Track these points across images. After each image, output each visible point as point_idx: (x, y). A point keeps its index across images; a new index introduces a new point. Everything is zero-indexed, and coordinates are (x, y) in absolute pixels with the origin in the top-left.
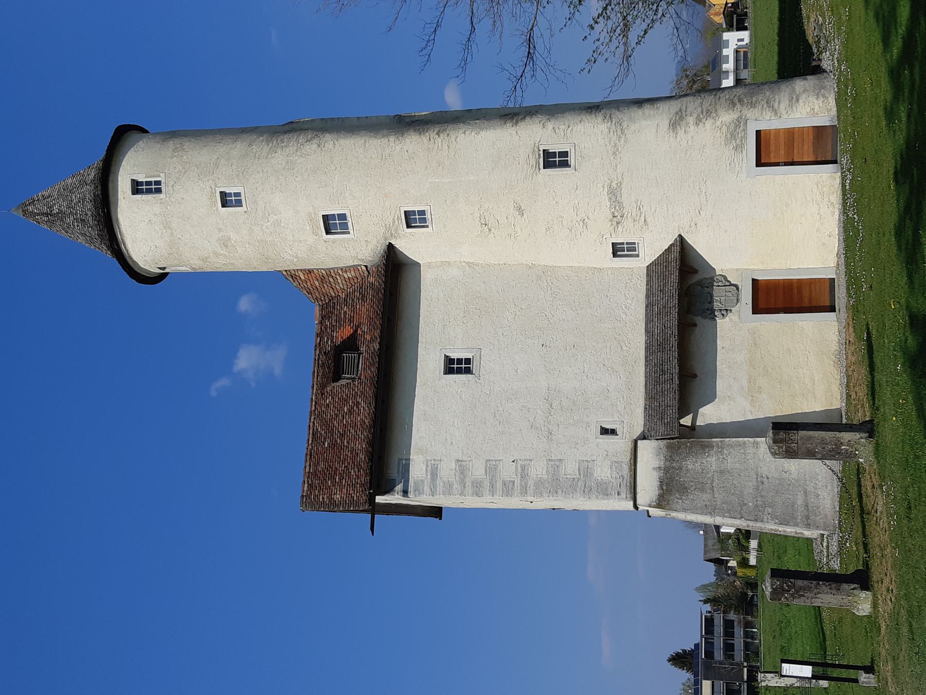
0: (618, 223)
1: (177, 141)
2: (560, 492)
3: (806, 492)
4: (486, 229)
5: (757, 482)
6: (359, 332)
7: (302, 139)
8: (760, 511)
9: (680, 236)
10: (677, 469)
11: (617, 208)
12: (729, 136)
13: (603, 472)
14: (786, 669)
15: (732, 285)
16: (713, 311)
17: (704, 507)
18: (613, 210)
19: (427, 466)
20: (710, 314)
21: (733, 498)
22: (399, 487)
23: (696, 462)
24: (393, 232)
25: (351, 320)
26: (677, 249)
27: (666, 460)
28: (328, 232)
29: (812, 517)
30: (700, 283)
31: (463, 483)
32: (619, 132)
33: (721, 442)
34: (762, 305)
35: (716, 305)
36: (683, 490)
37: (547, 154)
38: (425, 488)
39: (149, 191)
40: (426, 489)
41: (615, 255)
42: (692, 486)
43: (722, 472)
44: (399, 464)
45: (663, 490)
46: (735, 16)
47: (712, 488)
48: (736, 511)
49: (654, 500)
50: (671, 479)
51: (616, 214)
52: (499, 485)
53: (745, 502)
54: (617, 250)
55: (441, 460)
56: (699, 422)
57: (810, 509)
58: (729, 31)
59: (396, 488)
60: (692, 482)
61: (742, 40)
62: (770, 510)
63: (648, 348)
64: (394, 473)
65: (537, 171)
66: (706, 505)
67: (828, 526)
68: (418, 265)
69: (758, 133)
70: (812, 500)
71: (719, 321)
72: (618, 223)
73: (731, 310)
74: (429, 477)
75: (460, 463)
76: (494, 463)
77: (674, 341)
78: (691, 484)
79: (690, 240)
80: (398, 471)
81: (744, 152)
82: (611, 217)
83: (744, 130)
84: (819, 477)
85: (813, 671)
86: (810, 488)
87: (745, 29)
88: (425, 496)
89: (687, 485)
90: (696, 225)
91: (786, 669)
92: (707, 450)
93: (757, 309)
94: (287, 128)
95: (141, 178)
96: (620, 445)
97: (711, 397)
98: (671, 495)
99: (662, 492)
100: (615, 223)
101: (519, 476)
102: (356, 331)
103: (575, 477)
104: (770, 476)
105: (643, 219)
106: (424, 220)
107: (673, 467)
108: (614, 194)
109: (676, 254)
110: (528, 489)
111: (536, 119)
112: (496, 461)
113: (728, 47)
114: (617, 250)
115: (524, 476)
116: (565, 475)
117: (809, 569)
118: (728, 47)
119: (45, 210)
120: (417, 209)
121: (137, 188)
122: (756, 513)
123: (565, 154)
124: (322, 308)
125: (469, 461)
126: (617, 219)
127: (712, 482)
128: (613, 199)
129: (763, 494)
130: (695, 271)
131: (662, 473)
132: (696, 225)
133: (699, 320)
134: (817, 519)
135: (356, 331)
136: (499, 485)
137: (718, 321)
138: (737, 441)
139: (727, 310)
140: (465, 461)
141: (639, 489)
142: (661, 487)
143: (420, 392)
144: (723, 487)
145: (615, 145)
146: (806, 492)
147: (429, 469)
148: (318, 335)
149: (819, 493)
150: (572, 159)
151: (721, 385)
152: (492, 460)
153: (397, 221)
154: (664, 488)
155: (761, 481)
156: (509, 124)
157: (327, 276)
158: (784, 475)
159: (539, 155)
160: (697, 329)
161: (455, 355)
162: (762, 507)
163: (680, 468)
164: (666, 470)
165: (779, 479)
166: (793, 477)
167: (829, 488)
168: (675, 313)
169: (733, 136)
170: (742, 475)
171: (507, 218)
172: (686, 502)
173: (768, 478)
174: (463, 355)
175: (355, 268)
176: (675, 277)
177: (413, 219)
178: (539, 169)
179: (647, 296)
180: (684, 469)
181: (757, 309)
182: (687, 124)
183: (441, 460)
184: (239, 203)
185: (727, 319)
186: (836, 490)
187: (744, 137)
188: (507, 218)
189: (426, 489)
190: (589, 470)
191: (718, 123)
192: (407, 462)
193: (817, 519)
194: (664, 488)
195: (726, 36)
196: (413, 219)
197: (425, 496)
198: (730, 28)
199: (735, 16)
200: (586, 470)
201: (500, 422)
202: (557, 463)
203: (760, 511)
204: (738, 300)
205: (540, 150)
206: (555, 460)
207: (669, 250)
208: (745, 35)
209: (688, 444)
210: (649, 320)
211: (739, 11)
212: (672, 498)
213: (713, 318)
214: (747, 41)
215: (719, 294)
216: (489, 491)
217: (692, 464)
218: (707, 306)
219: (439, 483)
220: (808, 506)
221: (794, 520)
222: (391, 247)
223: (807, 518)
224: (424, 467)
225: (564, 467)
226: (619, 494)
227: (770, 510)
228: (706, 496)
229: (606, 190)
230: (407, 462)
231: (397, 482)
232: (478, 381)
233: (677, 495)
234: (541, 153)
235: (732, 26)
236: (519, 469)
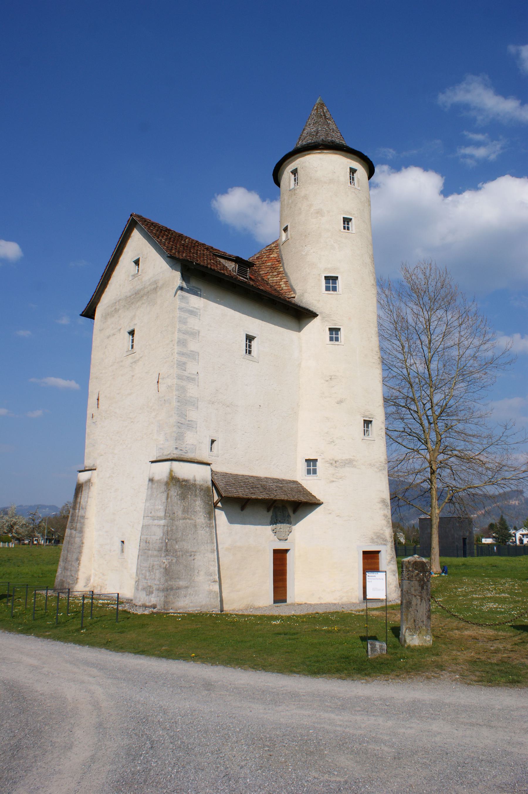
0: (331, 464)
2: (179, 404)
3: (187, 587)
4: (328, 379)
5: (191, 552)
8: (173, 553)
9: (322, 503)
10: (195, 493)
11: (341, 464)
12: (378, 535)
13: (190, 438)
14: (375, 576)
16: (276, 523)
17: (173, 512)
18: (340, 461)
19: (197, 309)
20: (274, 521)
21: (180, 534)
22: (184, 285)
23: (200, 508)
24: (326, 319)
27: (201, 486)
29: (172, 593)
30: (289, 516)
31: (186, 333)
32: (380, 468)
33: (213, 526)
35: (279, 526)
36: (183, 497)
38: (184, 304)
40: (183, 305)
42: (186, 504)
43: (195, 526)
44: (198, 288)
45: (182, 481)
47: (184, 519)
48: (172, 536)
49: (176, 475)
50: (189, 489)
51: (337, 463)
52: (184, 359)
53: (178, 543)
55: (200, 319)
56: (217, 511)
57: (178, 591)
59: (184, 283)
60: (188, 504)
62: (174, 561)
63: (258, 479)
64: (194, 283)
65: (362, 416)
66: (174, 513)
67: (167, 605)
68: (300, 330)
69: (378, 552)
70: (183, 592)
71: (269, 528)
72: (331, 464)
73: (275, 535)
74: (191, 309)
75: (198, 333)
76: (197, 358)
78: (187, 503)
80: (193, 287)
81: (370, 544)
82: (336, 459)
83: (381, 544)
84: (196, 597)
86: (190, 591)
88: (179, 302)
89: (186, 499)
90: (330, 513)
91: (375, 576)
92: (208, 516)
93: (276, 552)
96: (204, 454)
97: (231, 521)
98: (179, 487)
99: (181, 481)
100: (331, 462)
101: (189, 375)
103: (188, 417)
104: (195, 561)
105: (335, 480)
107: (196, 490)
108: (349, 463)
109: (314, 501)
110: (181, 380)
112: (198, 360)
114: (311, 463)
115: (190, 379)
116: (189, 410)
122: (172, 551)
125: (199, 340)
126: (334, 463)
127: (189, 519)
128: (346, 462)
129: (184, 556)
130: (295, 511)
131: (192, 482)
132: (330, 513)
133: (270, 513)
134: (171, 597)
136: (184, 359)
137: (270, 526)
138: (214, 538)
139: (276, 533)
140: (199, 338)
141: (182, 464)
142: (184, 481)
143: (237, 315)
144: (186, 527)
145: (374, 465)
146: (187, 587)
147: (195, 310)
149: (188, 598)
151: (238, 527)
152: (198, 357)
153: (334, 322)
154: (184, 483)
155: (192, 554)
158: (196, 571)
159: (369, 418)
160: (265, 512)
162: (176, 555)
163: (196, 496)
164: (194, 485)
165: (193, 568)
166: (196, 578)
167: (191, 605)
169: (378, 537)
170: (195, 540)
171: (336, 393)
172: (176, 498)
173: (194, 560)
177: (334, 332)
178: (364, 417)
180: (196, 498)
181: (276, 552)
182: (384, 509)
183: (200, 319)
185: (271, 532)
186: (190, 610)
187: (378, 544)
188: (336, 393)
189: (183, 305)
190: (191, 428)
191: (385, 528)
192: (199, 295)
193: (171, 597)
194: (184, 483)
196: (334, 332)
197: (179, 302)
200: (190, 425)
201: (220, 368)
202: (196, 404)
203: (173, 553)
204: (280, 540)
205: (372, 418)
206: (198, 404)
207: (309, 494)
209: (210, 503)
212: (178, 488)
215: (282, 527)
216: (180, 351)
217: (198, 504)
219: (186, 315)
220: (178, 589)
221: (169, 579)
222: (314, 315)
223: (172, 589)
224: (196, 306)
225: (193, 409)
226: (176, 448)
227: (174, 561)
228: (180, 513)
229: (352, 458)
230: (199, 295)
231: (188, 284)
232: (242, 357)
233: (179, 492)
234: (370, 420)
236: (193, 376)
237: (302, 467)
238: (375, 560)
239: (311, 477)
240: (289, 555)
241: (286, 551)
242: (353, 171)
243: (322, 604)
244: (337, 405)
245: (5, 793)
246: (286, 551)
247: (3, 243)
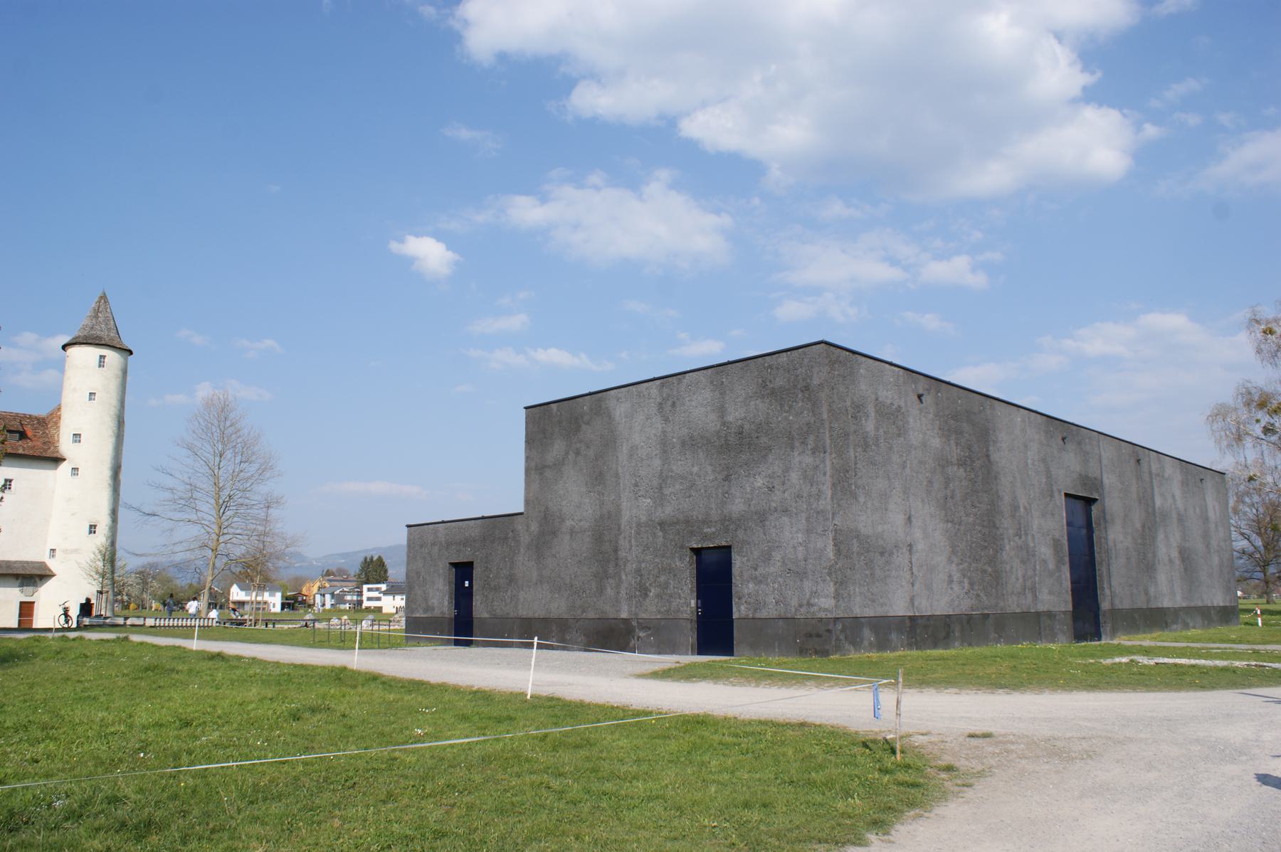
1: (121, 376)
6: (29, 441)
7: (115, 428)
15: (33, 593)
16: (22, 586)
20: (22, 585)
25: (35, 436)
26: (50, 573)
28: (74, 435)
30: (35, 582)
34: (23, 605)
35: (25, 588)
37: (95, 526)
39: (100, 362)
41: (51, 550)
46: (293, 601)
54: (53, 550)
58: (282, 597)
61: (274, 606)
63: (8, 562)
68: (56, 468)
77: (10, 572)
79: (54, 578)
85: (32, 621)
87: (283, 608)
93: (22, 603)
94: (121, 420)
95: (106, 359)
102: (29, 439)
106: (74, 474)
109: (48, 573)
111: (111, 523)
113: (270, 595)
117: (970, 742)
118: (270, 595)
119: (101, 309)
120: (79, 472)
121: (102, 357)
123: (95, 532)
124: (44, 419)
126: (66, 551)
130: (41, 580)
133: (19, 581)
135: (29, 439)
148: (30, 416)
150: (92, 535)
156: (110, 512)
157: (57, 425)
161: (13, 483)
168: (22, 572)
174: (13, 487)
175: (58, 441)
176: (38, 572)
179: (31, 562)
181: (22, 603)
184: (90, 399)
185: (20, 593)
195: (279, 595)
198: (285, 597)
199: (293, 601)
207: (50, 570)
208: (278, 609)
210: (21, 562)
211: (297, 605)
213: (19, 586)
214: (273, 610)
215: (29, 589)
218: (25, 584)
222: (65, 460)
235: (287, 599)
237: (48, 553)
238: (690, 652)
239: (52, 560)
240: (35, 604)
241: (34, 602)
242: (102, 357)
243: (816, 652)
244: (1255, 782)
245: (1, 694)
246: (34, 602)
247: (2, 468)
